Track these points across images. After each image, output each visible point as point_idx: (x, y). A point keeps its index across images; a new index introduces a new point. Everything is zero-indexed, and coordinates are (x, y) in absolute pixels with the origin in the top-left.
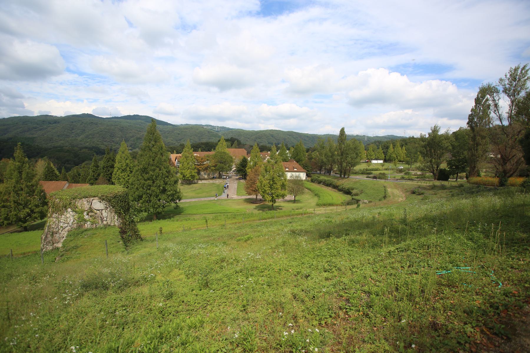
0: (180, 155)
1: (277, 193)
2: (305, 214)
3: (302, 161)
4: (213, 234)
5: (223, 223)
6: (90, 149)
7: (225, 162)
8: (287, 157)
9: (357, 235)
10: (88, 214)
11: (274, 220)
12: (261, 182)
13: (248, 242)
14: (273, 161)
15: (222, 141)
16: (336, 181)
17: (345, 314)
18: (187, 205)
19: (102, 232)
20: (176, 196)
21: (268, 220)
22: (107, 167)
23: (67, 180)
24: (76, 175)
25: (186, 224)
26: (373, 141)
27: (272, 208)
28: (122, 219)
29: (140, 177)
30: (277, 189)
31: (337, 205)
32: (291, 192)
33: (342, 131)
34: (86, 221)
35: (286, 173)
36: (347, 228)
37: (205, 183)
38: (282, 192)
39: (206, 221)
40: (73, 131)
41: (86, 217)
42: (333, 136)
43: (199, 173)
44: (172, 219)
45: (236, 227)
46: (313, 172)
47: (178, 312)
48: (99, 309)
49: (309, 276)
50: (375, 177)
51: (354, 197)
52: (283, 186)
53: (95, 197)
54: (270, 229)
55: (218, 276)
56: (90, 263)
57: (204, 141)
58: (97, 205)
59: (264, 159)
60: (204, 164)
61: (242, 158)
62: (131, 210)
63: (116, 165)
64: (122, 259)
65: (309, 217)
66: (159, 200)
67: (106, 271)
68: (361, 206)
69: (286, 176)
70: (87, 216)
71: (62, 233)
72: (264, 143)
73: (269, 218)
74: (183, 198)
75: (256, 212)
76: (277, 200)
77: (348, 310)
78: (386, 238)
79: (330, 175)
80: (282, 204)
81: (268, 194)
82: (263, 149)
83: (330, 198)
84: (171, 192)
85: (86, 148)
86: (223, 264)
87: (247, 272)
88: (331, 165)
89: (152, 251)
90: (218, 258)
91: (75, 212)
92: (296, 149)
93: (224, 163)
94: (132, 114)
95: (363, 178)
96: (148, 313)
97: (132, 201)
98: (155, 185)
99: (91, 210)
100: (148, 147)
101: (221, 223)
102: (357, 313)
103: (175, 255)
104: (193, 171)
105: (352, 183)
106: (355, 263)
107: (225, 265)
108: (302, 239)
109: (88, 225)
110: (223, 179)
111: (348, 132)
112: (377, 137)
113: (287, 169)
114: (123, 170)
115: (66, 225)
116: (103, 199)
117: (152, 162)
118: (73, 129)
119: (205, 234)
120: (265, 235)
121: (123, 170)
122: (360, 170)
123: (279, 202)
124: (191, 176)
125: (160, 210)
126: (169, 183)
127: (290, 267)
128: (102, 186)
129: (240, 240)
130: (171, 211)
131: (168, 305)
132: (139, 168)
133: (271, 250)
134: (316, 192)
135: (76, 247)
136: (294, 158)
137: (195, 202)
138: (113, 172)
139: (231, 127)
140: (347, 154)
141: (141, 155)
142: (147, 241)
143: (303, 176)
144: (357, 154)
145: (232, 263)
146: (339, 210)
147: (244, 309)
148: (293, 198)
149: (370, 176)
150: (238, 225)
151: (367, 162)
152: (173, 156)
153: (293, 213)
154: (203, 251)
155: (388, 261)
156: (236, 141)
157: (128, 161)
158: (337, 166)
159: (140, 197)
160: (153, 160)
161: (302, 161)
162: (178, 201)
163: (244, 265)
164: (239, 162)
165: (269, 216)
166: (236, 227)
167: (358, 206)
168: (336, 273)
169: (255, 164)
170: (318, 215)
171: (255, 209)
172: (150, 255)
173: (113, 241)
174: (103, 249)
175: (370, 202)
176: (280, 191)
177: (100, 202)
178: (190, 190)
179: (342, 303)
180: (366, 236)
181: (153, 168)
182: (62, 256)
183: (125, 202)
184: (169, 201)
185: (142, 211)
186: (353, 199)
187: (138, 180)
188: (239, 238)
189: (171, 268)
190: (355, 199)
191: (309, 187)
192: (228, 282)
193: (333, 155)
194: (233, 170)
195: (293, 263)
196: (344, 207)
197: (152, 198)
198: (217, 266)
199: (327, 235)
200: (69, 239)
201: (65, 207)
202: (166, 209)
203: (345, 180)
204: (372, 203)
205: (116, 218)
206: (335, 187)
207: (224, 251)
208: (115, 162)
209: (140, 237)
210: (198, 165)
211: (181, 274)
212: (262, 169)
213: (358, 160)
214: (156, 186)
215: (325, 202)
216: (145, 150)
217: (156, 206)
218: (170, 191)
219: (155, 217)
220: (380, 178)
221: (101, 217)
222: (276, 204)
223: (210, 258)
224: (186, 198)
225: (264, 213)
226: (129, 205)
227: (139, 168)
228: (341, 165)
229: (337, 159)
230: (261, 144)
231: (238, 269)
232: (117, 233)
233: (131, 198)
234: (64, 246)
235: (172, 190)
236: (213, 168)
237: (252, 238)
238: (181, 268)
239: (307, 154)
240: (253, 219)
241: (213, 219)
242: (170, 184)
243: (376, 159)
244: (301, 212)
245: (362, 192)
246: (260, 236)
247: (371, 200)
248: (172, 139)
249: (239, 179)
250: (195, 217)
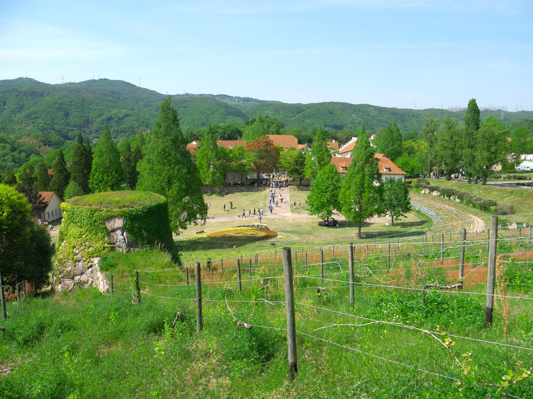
33: (473, 104)
111: (481, 105)
139: (261, 99)
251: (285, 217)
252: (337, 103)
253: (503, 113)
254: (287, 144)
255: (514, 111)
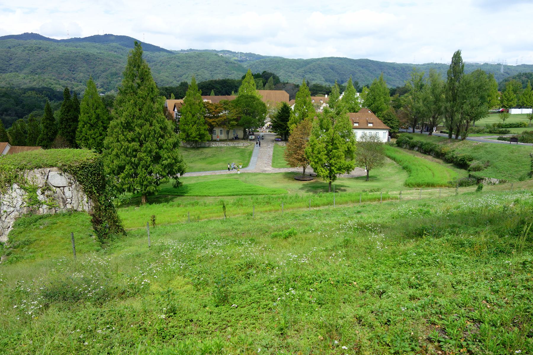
0: (181, 101)
1: (339, 164)
2: (384, 199)
3: (381, 110)
4: (235, 227)
5: (251, 210)
6: (40, 91)
7: (253, 112)
8: (356, 104)
9: (470, 234)
10: (43, 193)
11: (331, 208)
12: (313, 147)
13: (290, 240)
14: (333, 111)
15: (248, 77)
16: (441, 144)
17: (437, 349)
18: (193, 182)
19: (65, 220)
20: (174, 169)
21: (321, 208)
22: (67, 120)
23: (7, 141)
24: (20, 133)
25: (194, 211)
26: (516, 74)
27: (329, 188)
28: (95, 201)
29: (121, 137)
30: (339, 157)
31: (441, 186)
32: (362, 163)
33: (457, 57)
34: (40, 203)
35: (355, 131)
36: (456, 223)
37: (221, 146)
38: (348, 162)
39: (224, 207)
40: (11, 62)
41: (41, 198)
42: (440, 66)
43: (211, 131)
44: (171, 203)
45: (270, 216)
46: (401, 130)
47: (184, 335)
48: (72, 326)
49: (384, 292)
50: (514, 139)
51: (472, 173)
52: (349, 153)
53: (52, 166)
54: (324, 221)
55: (243, 288)
56: (52, 266)
57: (219, 77)
58: (57, 179)
59: (318, 107)
60: (218, 117)
61: (281, 106)
62: (108, 188)
63: (82, 117)
64: (97, 262)
65: (391, 204)
66: (150, 173)
67: (77, 276)
68: (485, 188)
69: (355, 136)
70: (42, 196)
71: (7, 220)
72: (319, 80)
73: (324, 205)
74: (187, 170)
75: (304, 194)
76: (338, 176)
77: (441, 344)
78: (521, 242)
79: (430, 134)
80: (346, 183)
81: (323, 166)
82: (316, 90)
83: (430, 173)
84: (169, 160)
85: (32, 89)
86: (249, 271)
87: (286, 283)
88: (434, 117)
89: (142, 250)
90: (242, 262)
91: (24, 189)
92: (372, 90)
93: (252, 114)
94: (102, 33)
95: (492, 140)
96: (141, 335)
97: (109, 174)
98: (143, 149)
99: (47, 187)
100: (132, 87)
101: (247, 211)
102: (458, 349)
103: (177, 255)
104: (202, 128)
105: (470, 149)
106: (464, 276)
107: (255, 272)
108: (377, 240)
109: (43, 210)
110: (251, 140)
111: (467, 58)
112: (524, 66)
113: (356, 125)
114: (92, 126)
115: (12, 209)
116: (65, 171)
117: (138, 113)
118: (11, 59)
119: (222, 227)
120: (317, 230)
121: (92, 126)
122: (488, 126)
123: (342, 179)
124: (199, 135)
125: (151, 188)
126: (164, 146)
127: (354, 279)
128: (62, 150)
129: (276, 236)
130: (169, 191)
131: (171, 324)
132: (119, 121)
133: (325, 253)
134: (406, 164)
135: (28, 243)
136: (369, 106)
137: (205, 177)
138: (76, 128)
139: (263, 54)
140: (464, 98)
141: (121, 102)
142: (133, 236)
143: (383, 136)
144: (482, 98)
145: (264, 271)
146: (444, 195)
147: (282, 333)
148: (363, 172)
149: (505, 136)
150: (273, 214)
151: (502, 112)
152: (170, 103)
153: (364, 196)
154: (219, 252)
155: (520, 277)
156: (272, 77)
157: (98, 111)
158: (444, 120)
159: (121, 169)
160: (140, 110)
161: (381, 110)
162: (178, 175)
163: (283, 273)
164: (276, 113)
165: (325, 200)
166: (270, 216)
167: (480, 188)
168: (428, 291)
169: (304, 116)
170: (407, 201)
171: (302, 189)
172: (138, 256)
173: (82, 235)
174: (67, 246)
175: (502, 182)
176: (343, 161)
177: (61, 174)
178: (197, 158)
179: (434, 334)
180: (485, 236)
181: (139, 122)
182: (8, 255)
183: (99, 175)
184: (165, 174)
185: (124, 191)
186: (470, 176)
187: (118, 141)
188: (276, 233)
189: (171, 275)
190: (474, 177)
191: (393, 155)
192: (257, 295)
193: (437, 100)
194: (266, 125)
195: (360, 273)
196: (453, 189)
197: (139, 171)
198: (241, 273)
199: (419, 234)
200: (18, 230)
201: (9, 181)
202: (160, 188)
203: (457, 144)
204: (506, 184)
205: (86, 199)
206: (439, 155)
207: (253, 253)
208: (79, 112)
209: (122, 230)
210: (210, 118)
211: (188, 283)
212: (315, 124)
213: (483, 108)
214: (145, 152)
215: (419, 181)
216: (127, 94)
217: (145, 183)
218: (166, 159)
219: (144, 200)
220: (523, 140)
221: (63, 198)
222: (336, 183)
223: (229, 262)
224: (192, 170)
225: (316, 196)
226: (104, 180)
227: (119, 121)
228: (452, 118)
229: (446, 108)
230: (314, 83)
231: (273, 277)
232: (88, 223)
233: (107, 170)
234: (10, 241)
235: (169, 158)
236: (235, 123)
237: (295, 234)
238: (187, 274)
239: (392, 98)
240: (298, 205)
241: (234, 204)
242: (166, 148)
243: (520, 107)
244: (378, 196)
245: (488, 164)
246: (308, 231)
247: (504, 179)
248: (167, 74)
249: (277, 140)
250: (202, 201)
251: (265, 171)
252: (337, 58)
253: (502, 67)
254: (272, 100)
255: (515, 65)
